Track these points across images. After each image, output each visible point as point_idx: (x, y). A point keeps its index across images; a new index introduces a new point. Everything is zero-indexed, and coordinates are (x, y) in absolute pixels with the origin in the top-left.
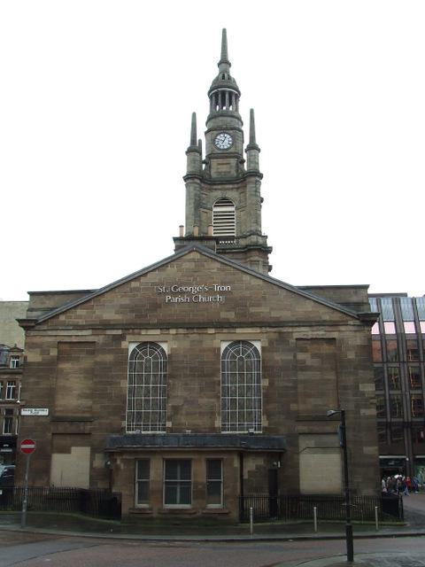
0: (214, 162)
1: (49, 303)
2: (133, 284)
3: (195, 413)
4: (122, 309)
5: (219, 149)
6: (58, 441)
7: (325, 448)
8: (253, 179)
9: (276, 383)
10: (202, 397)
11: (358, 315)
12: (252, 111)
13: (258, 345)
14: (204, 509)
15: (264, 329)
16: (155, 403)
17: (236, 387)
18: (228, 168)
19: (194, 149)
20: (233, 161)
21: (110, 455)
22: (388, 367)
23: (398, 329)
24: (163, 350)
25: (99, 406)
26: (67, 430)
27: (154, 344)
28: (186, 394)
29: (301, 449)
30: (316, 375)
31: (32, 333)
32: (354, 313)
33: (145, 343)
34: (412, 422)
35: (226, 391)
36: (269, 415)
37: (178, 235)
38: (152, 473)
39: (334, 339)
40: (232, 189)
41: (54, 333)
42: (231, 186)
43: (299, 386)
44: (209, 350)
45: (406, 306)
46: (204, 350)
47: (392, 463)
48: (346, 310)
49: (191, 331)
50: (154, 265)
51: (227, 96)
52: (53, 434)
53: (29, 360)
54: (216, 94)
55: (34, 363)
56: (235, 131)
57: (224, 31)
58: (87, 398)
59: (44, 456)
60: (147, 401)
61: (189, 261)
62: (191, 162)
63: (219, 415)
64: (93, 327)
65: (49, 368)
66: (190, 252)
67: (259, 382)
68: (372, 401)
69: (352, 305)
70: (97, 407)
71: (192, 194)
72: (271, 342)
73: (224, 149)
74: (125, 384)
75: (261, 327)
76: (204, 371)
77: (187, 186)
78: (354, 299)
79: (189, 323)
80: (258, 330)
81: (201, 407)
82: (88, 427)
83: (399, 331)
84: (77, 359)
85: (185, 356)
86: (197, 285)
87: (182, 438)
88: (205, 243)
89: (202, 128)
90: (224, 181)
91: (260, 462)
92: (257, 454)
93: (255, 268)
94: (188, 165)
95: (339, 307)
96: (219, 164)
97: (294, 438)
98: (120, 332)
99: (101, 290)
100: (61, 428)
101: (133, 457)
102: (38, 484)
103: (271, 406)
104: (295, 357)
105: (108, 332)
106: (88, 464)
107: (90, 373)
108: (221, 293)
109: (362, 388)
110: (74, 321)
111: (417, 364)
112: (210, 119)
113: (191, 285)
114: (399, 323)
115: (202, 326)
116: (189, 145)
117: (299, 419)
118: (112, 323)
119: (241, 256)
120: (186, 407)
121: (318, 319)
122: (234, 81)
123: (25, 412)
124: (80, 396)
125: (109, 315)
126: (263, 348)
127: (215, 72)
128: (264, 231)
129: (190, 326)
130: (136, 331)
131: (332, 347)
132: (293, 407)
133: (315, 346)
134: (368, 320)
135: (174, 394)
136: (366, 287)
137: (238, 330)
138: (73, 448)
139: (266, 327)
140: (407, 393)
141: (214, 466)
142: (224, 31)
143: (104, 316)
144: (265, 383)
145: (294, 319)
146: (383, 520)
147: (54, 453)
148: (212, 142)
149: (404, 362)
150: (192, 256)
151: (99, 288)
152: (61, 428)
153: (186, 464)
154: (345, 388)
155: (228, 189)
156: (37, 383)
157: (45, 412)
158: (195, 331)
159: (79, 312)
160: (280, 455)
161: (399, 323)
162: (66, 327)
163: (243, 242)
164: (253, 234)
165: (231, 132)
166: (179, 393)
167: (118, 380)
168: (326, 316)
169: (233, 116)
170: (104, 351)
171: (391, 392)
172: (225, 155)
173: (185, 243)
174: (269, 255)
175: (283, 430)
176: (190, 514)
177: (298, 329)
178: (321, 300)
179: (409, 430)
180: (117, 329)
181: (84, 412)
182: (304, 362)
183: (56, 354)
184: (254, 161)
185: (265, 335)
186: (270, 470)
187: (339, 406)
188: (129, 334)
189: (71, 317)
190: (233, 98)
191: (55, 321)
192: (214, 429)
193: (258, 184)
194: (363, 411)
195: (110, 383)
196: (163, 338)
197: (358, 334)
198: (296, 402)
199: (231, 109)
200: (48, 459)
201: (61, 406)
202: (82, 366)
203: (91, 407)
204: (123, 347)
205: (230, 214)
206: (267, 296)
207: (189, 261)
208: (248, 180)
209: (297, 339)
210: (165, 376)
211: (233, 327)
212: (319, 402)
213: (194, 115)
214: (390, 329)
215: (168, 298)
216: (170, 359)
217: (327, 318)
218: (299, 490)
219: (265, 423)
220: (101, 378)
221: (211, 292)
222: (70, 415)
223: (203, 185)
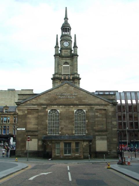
0: (63, 51)
1: (24, 97)
2: (49, 93)
4: (46, 100)
5: (65, 46)
7: (103, 139)
8: (75, 57)
10: (69, 125)
12: (75, 35)
13: (85, 111)
15: (86, 106)
16: (56, 127)
18: (67, 53)
19: (57, 47)
20: (69, 51)
26: (31, 134)
27: (55, 110)
28: (65, 124)
32: (111, 102)
33: (52, 110)
34: (130, 130)
36: (88, 130)
38: (61, 146)
39: (106, 109)
42: (68, 58)
43: (96, 122)
46: (70, 112)
48: (109, 101)
49: (66, 106)
51: (67, 29)
52: (27, 135)
54: (64, 29)
57: (66, 8)
58: (36, 125)
59: (24, 142)
60: (54, 126)
61: (65, 86)
64: (37, 105)
65: (25, 116)
69: (108, 97)
70: (39, 128)
72: (88, 110)
74: (48, 121)
75: (86, 106)
76: (70, 118)
77: (55, 58)
82: (37, 133)
84: (33, 114)
86: (68, 93)
88: (70, 81)
89: (59, 40)
91: (87, 143)
92: (87, 141)
95: (107, 100)
97: (94, 137)
98: (45, 106)
102: (23, 149)
103: (88, 128)
104: (95, 114)
105: (42, 106)
106: (37, 144)
107: (37, 118)
110: (32, 103)
113: (65, 93)
115: (69, 105)
116: (65, 17)
118: (43, 104)
121: (101, 104)
123: (18, 129)
124: (34, 125)
125: (42, 101)
126: (86, 111)
128: (79, 73)
129: (65, 105)
130: (50, 106)
132: (94, 128)
133: (100, 111)
137: (79, 106)
138: (32, 139)
141: (77, 144)
142: (66, 8)
144: (87, 121)
145: (95, 103)
151: (40, 93)
152: (29, 134)
153: (70, 144)
154: (108, 123)
156: (22, 121)
157: (24, 129)
158: (67, 106)
159: (33, 100)
160: (90, 141)
162: (30, 104)
165: (68, 41)
166: (63, 124)
169: (69, 36)
170: (41, 112)
172: (67, 48)
173: (64, 81)
174: (80, 80)
175: (92, 134)
176: (71, 157)
181: (35, 129)
182: (97, 115)
184: (76, 51)
185: (87, 108)
186: (89, 145)
190: (69, 30)
191: (26, 103)
192: (72, 134)
193: (77, 58)
194: (113, 129)
195: (43, 121)
197: (112, 108)
198: (95, 127)
199: (68, 34)
201: (28, 129)
203: (38, 128)
206: (87, 97)
207: (65, 86)
209: (96, 109)
211: (78, 106)
212: (101, 126)
213: (57, 35)
215: (59, 97)
217: (104, 103)
219: (87, 132)
221: (72, 95)
223: (60, 58)
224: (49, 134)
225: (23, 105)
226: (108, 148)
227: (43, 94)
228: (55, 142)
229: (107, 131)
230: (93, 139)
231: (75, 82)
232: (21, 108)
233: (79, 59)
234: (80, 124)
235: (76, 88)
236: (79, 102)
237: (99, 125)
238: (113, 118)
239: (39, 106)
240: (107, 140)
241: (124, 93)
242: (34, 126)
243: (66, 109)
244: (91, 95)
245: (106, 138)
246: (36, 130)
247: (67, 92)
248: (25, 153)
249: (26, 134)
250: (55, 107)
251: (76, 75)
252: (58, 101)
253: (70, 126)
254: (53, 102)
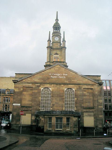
1: (21, 76)
2: (43, 73)
4: (40, 79)
5: (55, 41)
7: (90, 116)
8: (64, 48)
9: (78, 99)
13: (74, 89)
14: (66, 130)
18: (58, 46)
19: (49, 40)
24: (50, 90)
26: (25, 109)
31: (16, 84)
32: (97, 82)
36: (76, 107)
38: (52, 121)
41: (22, 84)
42: (58, 50)
44: (62, 90)
46: (60, 90)
48: (95, 81)
49: (57, 85)
58: (29, 101)
64: (32, 83)
65: (21, 93)
70: (33, 104)
72: (77, 89)
76: (61, 96)
78: (97, 79)
80: (74, 86)
82: (31, 109)
83: (111, 89)
84: (28, 91)
85: (56, 91)
86: (59, 73)
88: (61, 63)
89: (51, 36)
95: (94, 81)
97: (82, 113)
98: (39, 85)
101: (47, 117)
102: (17, 123)
103: (77, 105)
104: (83, 93)
105: (36, 85)
107: (31, 95)
113: (57, 73)
115: (60, 84)
117: (84, 108)
120: (56, 104)
125: (36, 80)
126: (75, 90)
127: (55, 22)
129: (57, 84)
131: (92, 91)
132: (82, 105)
134: (101, 84)
137: (69, 85)
141: (68, 119)
143: (35, 80)
146: (8, 133)
148: (53, 39)
154: (95, 101)
155: (57, 51)
156: (17, 97)
157: (19, 105)
158: (58, 85)
159: (28, 79)
162: (25, 83)
165: (58, 37)
167: (38, 97)
168: (91, 83)
170: (35, 89)
171: (107, 104)
172: (57, 42)
173: (56, 63)
177: (84, 86)
181: (29, 105)
182: (85, 94)
183: (22, 90)
188: (42, 85)
193: (65, 50)
194: (99, 107)
196: (50, 86)
197: (98, 88)
202: (29, 93)
204: (40, 88)
205: (57, 57)
213: (50, 32)
215: (51, 77)
217: (91, 83)
220: (34, 96)
232: (18, 86)
235: (66, 69)
237: (87, 103)
240: (94, 117)
250: (48, 86)
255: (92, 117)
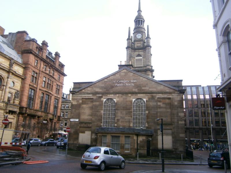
2: (106, 80)
3: (124, 122)
6: (82, 129)
8: (148, 48)
11: (179, 90)
12: (148, 26)
13: (145, 100)
14: (124, 152)
15: (147, 95)
17: (137, 113)
21: (96, 134)
22: (194, 110)
23: (198, 97)
24: (114, 101)
25: (94, 118)
26: (84, 126)
28: (121, 115)
29: (158, 134)
30: (162, 110)
31: (74, 95)
35: (134, 115)
36: (148, 122)
37: (120, 64)
38: (107, 140)
39: (170, 98)
40: (141, 51)
41: (81, 95)
42: (141, 50)
45: (200, 90)
46: (127, 101)
47: (195, 141)
48: (174, 88)
49: (123, 95)
50: (112, 74)
51: (140, 21)
52: (80, 127)
53: (73, 104)
54: (137, 21)
55: (74, 105)
56: (142, 33)
62: (128, 43)
63: (132, 122)
65: (78, 106)
66: (123, 70)
67: (145, 112)
68: (183, 119)
69: (177, 87)
70: (93, 119)
71: (128, 53)
72: (149, 99)
73: (139, 39)
74: (102, 112)
75: (146, 94)
76: (127, 108)
79: (123, 93)
80: (145, 95)
81: (126, 120)
83: (198, 98)
84: (88, 104)
85: (121, 103)
86: (126, 80)
87: (117, 129)
89: (132, 32)
90: (139, 49)
91: (144, 138)
92: (143, 135)
93: (148, 76)
94: (127, 44)
95: (172, 87)
96: (137, 43)
98: (101, 95)
99: (95, 82)
100: (82, 125)
102: (75, 142)
103: (149, 120)
104: (157, 104)
105: (97, 95)
107: (92, 108)
108: (133, 83)
109: (180, 114)
111: (204, 109)
112: (135, 29)
113: (123, 80)
114: (198, 95)
115: (127, 93)
116: (128, 37)
118: (99, 92)
119: (144, 73)
120: (121, 119)
122: (143, 17)
123: (71, 120)
125: (98, 90)
126: (146, 101)
127: (136, 14)
131: (170, 101)
133: (164, 100)
135: (117, 115)
136: (181, 81)
137: (138, 95)
138: (86, 132)
139: (147, 94)
140: (201, 118)
144: (147, 112)
145: (157, 91)
147: (80, 133)
148: (135, 37)
149: (200, 108)
150: (124, 71)
154: (174, 114)
156: (75, 111)
157: (77, 120)
158: (125, 95)
159: (89, 89)
161: (198, 95)
162: (84, 93)
163: (144, 68)
164: (148, 66)
165: (141, 33)
166: (119, 115)
168: (168, 90)
170: (96, 101)
172: (140, 40)
173: (122, 67)
177: (158, 95)
178: (166, 85)
179: (201, 130)
180: (100, 94)
182: (160, 105)
183: (81, 102)
184: (148, 42)
185: (147, 96)
187: (172, 120)
189: (86, 90)
190: (142, 22)
191: (81, 92)
194: (180, 122)
195: (97, 111)
200: (78, 135)
201: (82, 118)
203: (91, 119)
205: (141, 60)
207: (123, 72)
208: (146, 48)
209: (158, 98)
210: (115, 109)
211: (137, 94)
213: (129, 28)
214: (195, 97)
216: (116, 104)
217: (168, 91)
218: (158, 148)
219: (147, 125)
220: (95, 110)
222: (85, 121)
223: (132, 50)
224: (103, 126)
225: (78, 94)
226: (173, 146)
227: (99, 81)
228: (101, 135)
229: (172, 125)
230: (155, 134)
231: (148, 73)
233: (153, 51)
234: (139, 116)
235: (135, 75)
236: (138, 89)
238: (179, 109)
239: (94, 95)
240: (172, 136)
241: (207, 87)
242: (88, 117)
243: (124, 98)
244: (152, 82)
245: (171, 133)
246: (90, 121)
247: (125, 78)
248: (77, 147)
249: (80, 125)
251: (148, 67)
252: (114, 89)
253: (127, 118)
254: (109, 90)
255: (169, 137)
